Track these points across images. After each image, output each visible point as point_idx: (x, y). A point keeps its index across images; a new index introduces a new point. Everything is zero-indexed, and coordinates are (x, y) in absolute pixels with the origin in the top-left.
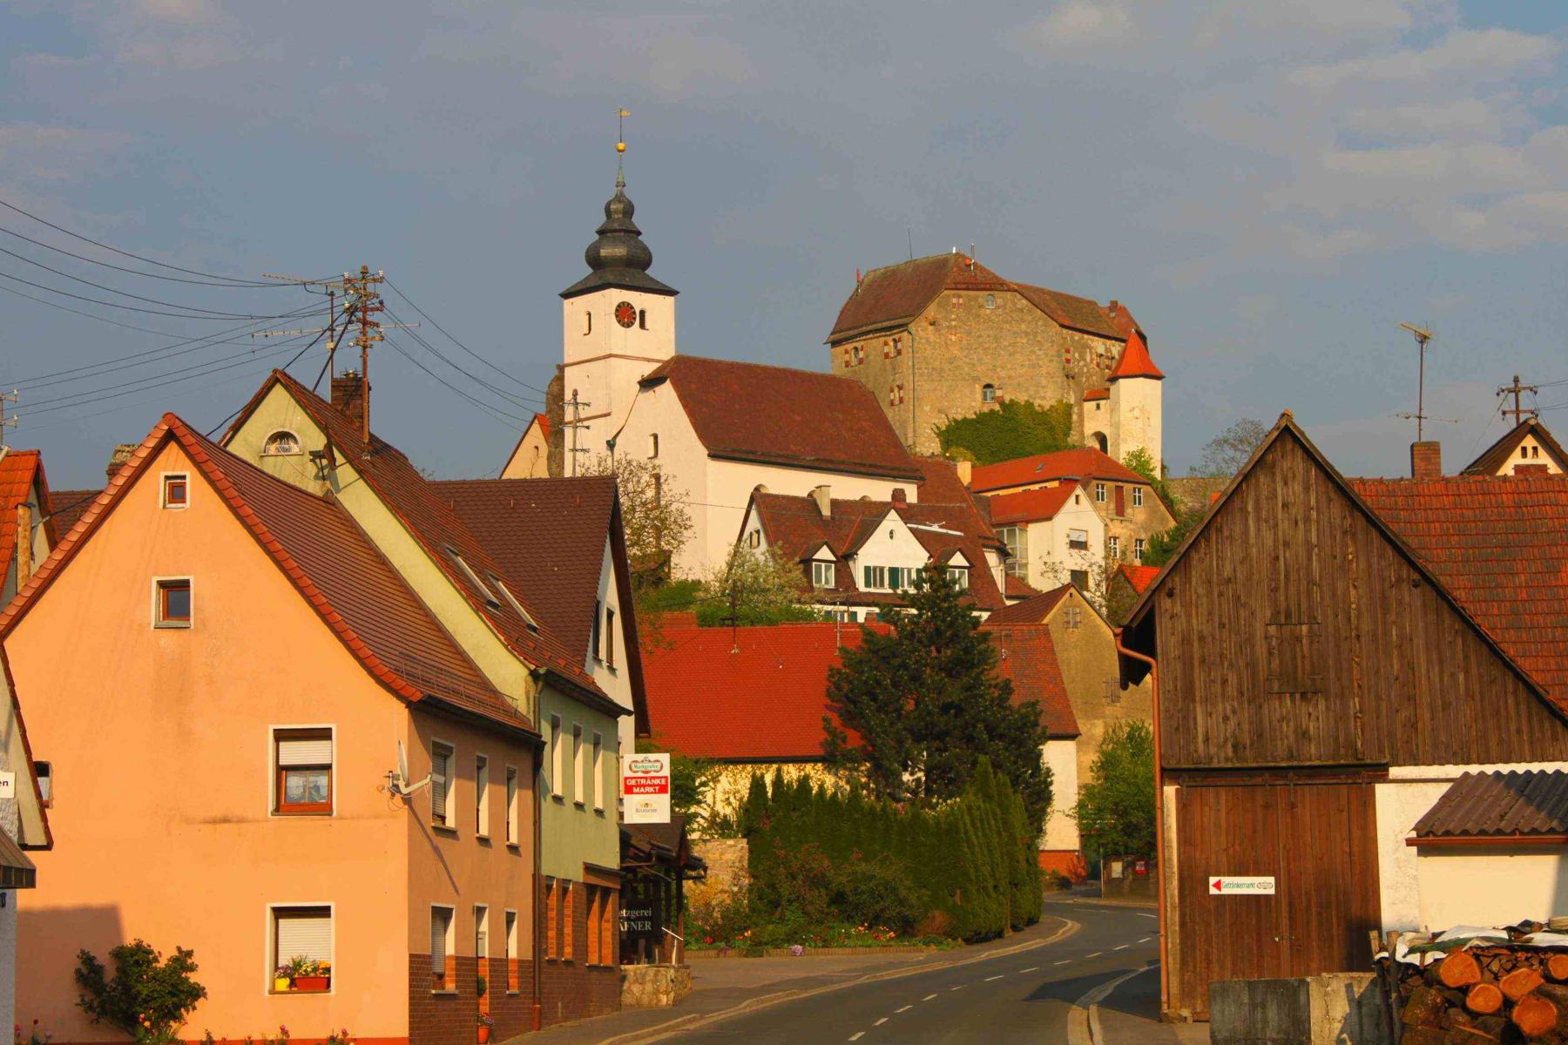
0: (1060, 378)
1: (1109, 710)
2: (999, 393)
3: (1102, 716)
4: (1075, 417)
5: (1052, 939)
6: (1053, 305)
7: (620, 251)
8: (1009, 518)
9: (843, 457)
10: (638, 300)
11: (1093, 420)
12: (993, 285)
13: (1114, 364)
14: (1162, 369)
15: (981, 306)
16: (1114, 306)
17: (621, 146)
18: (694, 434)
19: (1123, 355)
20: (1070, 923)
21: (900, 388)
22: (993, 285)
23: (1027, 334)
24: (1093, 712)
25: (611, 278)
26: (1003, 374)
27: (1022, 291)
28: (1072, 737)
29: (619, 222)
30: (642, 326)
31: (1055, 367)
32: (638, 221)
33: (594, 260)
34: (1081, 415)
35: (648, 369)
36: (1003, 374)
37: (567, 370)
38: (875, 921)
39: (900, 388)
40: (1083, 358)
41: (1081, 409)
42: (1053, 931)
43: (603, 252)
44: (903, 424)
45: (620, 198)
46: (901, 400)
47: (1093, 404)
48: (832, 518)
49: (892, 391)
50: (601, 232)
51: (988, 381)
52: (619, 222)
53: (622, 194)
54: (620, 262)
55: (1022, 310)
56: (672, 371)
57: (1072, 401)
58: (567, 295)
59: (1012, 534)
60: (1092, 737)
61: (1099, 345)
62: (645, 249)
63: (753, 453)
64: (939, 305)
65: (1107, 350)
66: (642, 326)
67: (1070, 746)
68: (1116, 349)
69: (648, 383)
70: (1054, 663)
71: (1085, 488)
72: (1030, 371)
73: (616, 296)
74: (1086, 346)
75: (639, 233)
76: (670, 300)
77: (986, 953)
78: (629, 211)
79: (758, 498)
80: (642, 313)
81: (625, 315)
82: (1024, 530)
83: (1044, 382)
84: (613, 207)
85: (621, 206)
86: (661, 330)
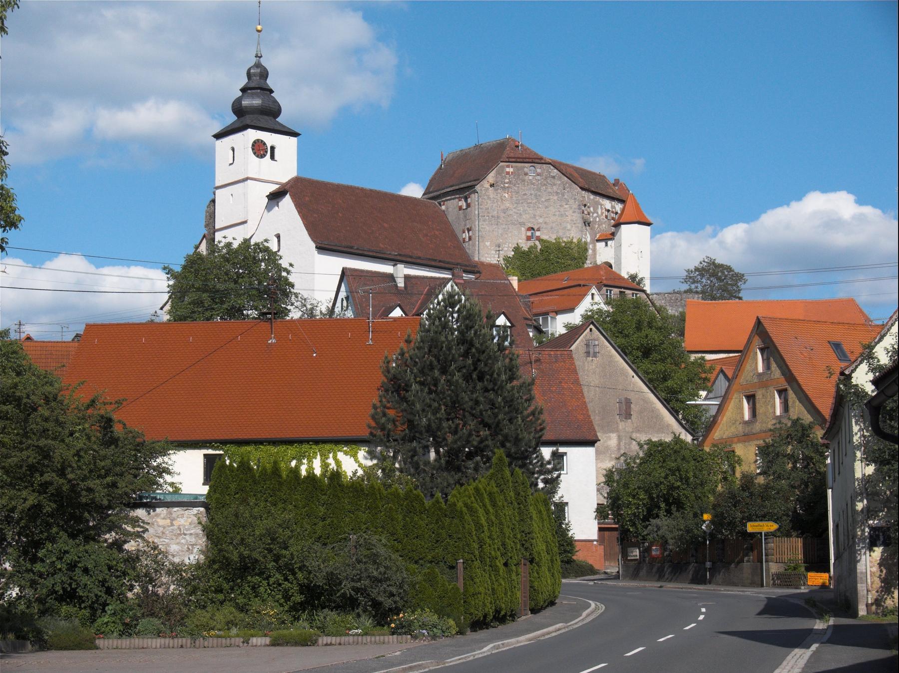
0: (580, 223)
1: (622, 425)
2: (538, 234)
3: (616, 430)
4: (590, 251)
5: (576, 623)
6: (576, 175)
7: (257, 102)
8: (544, 310)
9: (420, 254)
10: (269, 139)
11: (603, 254)
12: (535, 160)
13: (617, 217)
14: (650, 219)
15: (526, 174)
16: (617, 182)
17: (259, 28)
18: (306, 232)
19: (623, 210)
20: (593, 605)
21: (469, 230)
22: (535, 160)
23: (557, 193)
24: (610, 428)
25: (248, 122)
26: (541, 220)
27: (555, 165)
28: (591, 443)
29: (258, 81)
30: (272, 157)
31: (577, 217)
32: (270, 82)
33: (238, 109)
34: (594, 250)
35: (273, 188)
36: (541, 220)
37: (218, 192)
38: (348, 604)
39: (469, 230)
40: (595, 211)
41: (595, 246)
42: (576, 611)
43: (245, 103)
44: (473, 253)
45: (258, 65)
46: (470, 238)
47: (604, 244)
48: (406, 286)
49: (464, 232)
50: (243, 90)
51: (530, 225)
52: (258, 81)
53: (259, 62)
54: (256, 110)
55: (553, 177)
56: (292, 187)
57: (589, 240)
58: (219, 136)
59: (545, 321)
60: (607, 448)
61: (607, 204)
62: (275, 102)
63: (352, 248)
64: (498, 173)
65: (613, 207)
66: (272, 157)
67: (590, 451)
68: (619, 207)
69: (275, 197)
70: (577, 382)
71: (599, 290)
72: (559, 217)
73: (252, 135)
74: (598, 203)
75: (271, 91)
76: (294, 140)
77: (489, 646)
78: (264, 74)
79: (344, 272)
80: (273, 148)
81: (259, 149)
82: (553, 318)
83: (569, 227)
84: (252, 71)
85: (258, 70)
86: (286, 160)
